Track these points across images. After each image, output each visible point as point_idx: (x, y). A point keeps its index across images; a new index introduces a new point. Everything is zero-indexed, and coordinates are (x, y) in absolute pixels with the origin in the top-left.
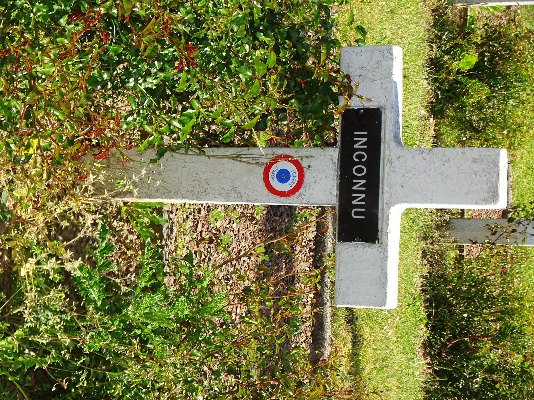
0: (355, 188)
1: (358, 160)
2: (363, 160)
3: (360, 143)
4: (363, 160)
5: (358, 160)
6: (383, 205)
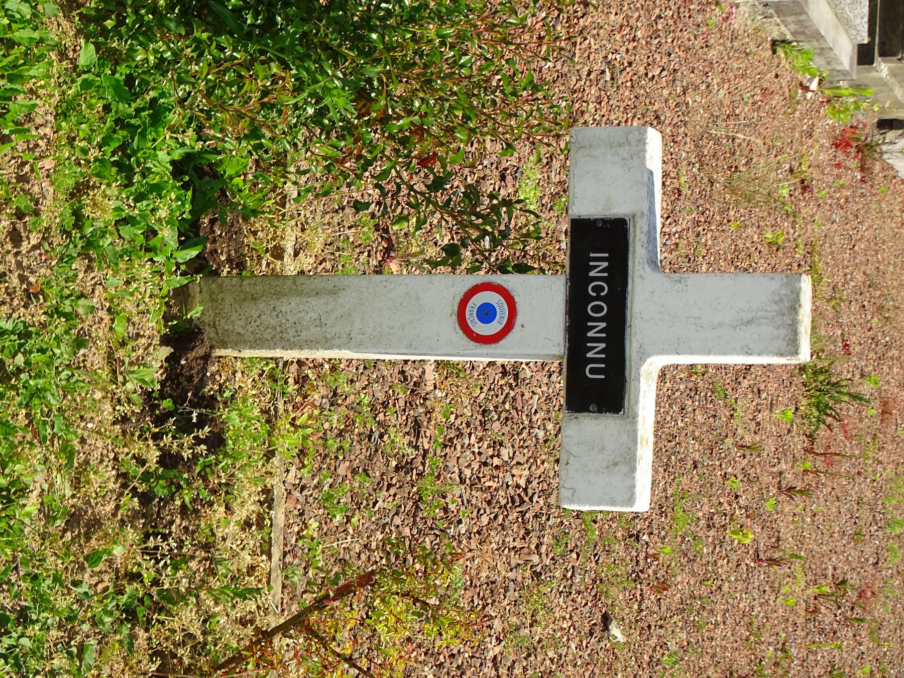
0: (603, 346)
1: (594, 294)
2: (602, 294)
3: (599, 268)
4: (602, 294)
5: (594, 294)
6: (651, 240)
